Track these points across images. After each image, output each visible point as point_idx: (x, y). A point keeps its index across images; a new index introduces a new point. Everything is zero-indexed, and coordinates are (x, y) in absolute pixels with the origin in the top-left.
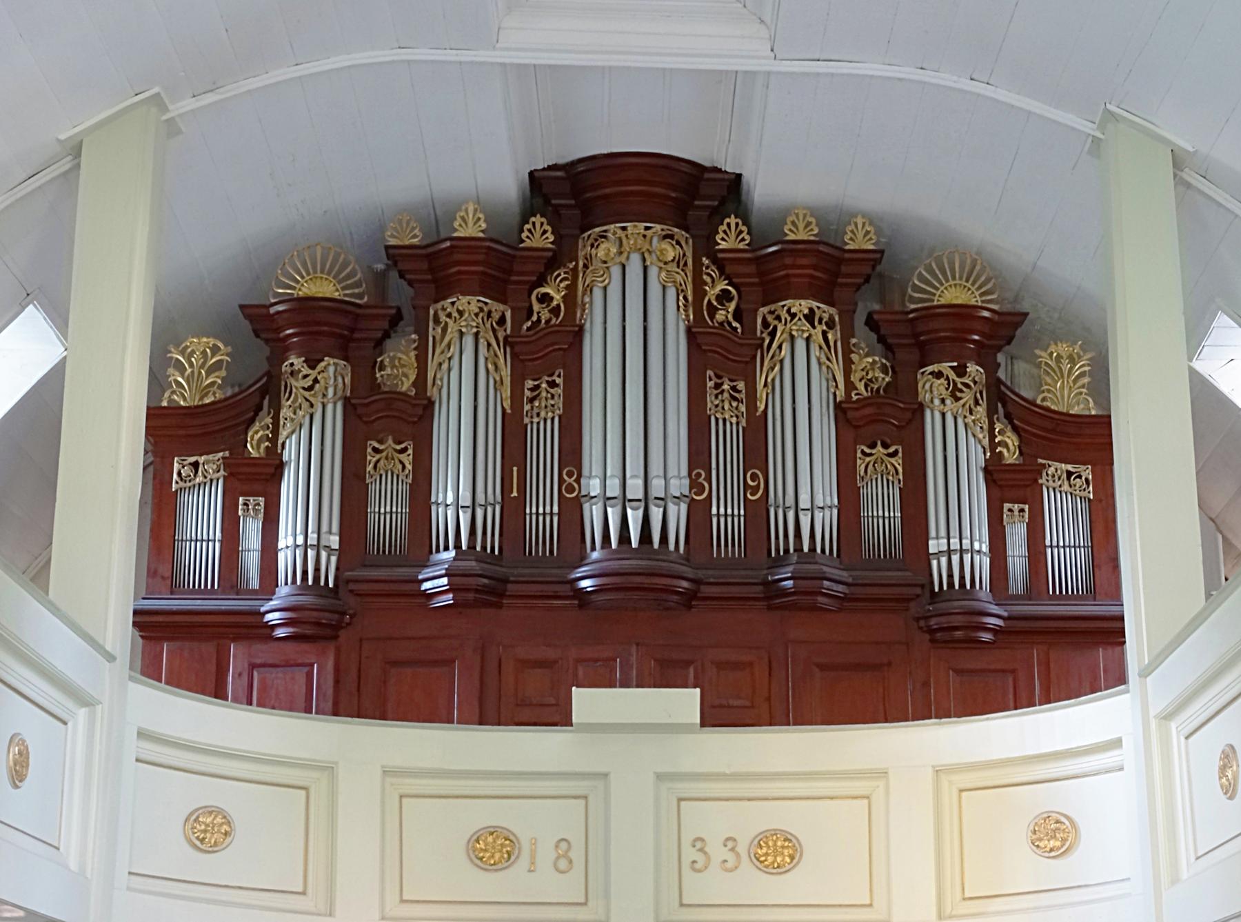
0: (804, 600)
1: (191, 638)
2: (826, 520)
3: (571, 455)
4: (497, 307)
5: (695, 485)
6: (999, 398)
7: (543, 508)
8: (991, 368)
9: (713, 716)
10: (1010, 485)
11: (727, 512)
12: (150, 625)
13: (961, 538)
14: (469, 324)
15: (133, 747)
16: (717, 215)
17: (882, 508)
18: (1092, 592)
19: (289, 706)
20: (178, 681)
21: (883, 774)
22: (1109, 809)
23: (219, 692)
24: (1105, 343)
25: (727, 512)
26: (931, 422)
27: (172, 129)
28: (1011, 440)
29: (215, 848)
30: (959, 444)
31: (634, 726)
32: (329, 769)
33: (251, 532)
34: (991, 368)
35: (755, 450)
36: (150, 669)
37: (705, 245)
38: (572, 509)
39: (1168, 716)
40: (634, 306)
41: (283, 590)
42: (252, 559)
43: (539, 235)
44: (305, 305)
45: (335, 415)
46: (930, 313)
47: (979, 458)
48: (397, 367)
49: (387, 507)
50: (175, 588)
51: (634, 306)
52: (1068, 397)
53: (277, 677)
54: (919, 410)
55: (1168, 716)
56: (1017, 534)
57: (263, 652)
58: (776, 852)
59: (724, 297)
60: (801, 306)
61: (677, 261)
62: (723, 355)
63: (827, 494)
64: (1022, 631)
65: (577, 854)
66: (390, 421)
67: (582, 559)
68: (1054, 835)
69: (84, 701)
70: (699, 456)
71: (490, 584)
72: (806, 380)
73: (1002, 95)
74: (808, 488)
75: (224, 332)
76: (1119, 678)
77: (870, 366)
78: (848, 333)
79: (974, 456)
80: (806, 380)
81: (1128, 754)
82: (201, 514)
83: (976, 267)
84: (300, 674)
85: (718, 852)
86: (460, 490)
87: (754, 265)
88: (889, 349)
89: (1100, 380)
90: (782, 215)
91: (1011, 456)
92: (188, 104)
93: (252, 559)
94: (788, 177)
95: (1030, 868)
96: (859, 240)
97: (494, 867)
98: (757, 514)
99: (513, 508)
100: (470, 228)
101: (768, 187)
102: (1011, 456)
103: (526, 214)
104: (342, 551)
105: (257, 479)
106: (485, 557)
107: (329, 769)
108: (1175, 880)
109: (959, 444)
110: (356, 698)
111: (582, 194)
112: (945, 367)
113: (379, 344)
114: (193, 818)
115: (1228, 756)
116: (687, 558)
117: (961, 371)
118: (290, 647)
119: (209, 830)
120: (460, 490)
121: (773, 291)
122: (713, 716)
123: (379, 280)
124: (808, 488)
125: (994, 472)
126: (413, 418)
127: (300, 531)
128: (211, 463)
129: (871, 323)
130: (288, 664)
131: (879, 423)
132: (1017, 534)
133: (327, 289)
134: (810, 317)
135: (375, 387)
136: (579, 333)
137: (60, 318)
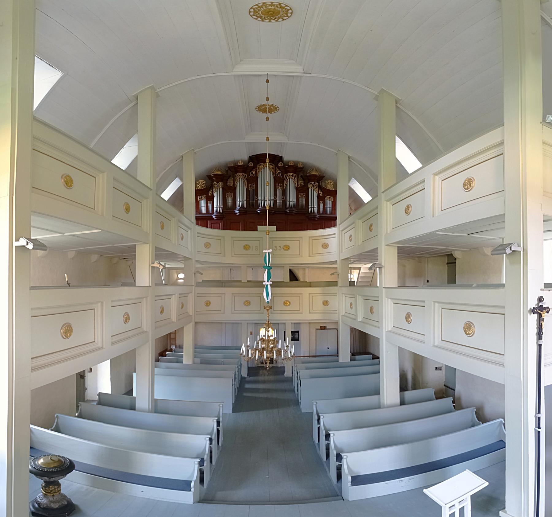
0: (291, 214)
1: (203, 220)
2: (294, 203)
3: (256, 194)
4: (245, 175)
5: (275, 198)
6: (320, 187)
7: (252, 201)
8: (319, 183)
9: (278, 230)
10: (321, 199)
11: (279, 202)
12: (197, 219)
13: (314, 206)
14: (241, 177)
15: (197, 235)
16: (278, 162)
17: (302, 201)
18: (332, 213)
19: (217, 229)
20: (201, 225)
21: (302, 238)
22: (333, 243)
23: (207, 227)
24: (336, 180)
25: (279, 202)
26: (310, 190)
27: (195, 153)
28: (321, 193)
29: (209, 248)
30: (314, 193)
31: (267, 231)
32: (224, 237)
33: (210, 206)
34: (319, 183)
35: (284, 193)
36: (197, 224)
37: (276, 166)
38: (257, 201)
39: (342, 231)
40: (266, 175)
41: (215, 213)
42: (210, 209)
43: (251, 165)
44: (216, 175)
45: (221, 190)
46: (310, 176)
47: (317, 195)
48: (230, 183)
49: (229, 201)
50: (200, 213)
51: (266, 175)
52: (330, 187)
53: (215, 225)
54: (308, 189)
55: (342, 231)
56: (321, 205)
57: (213, 221)
58: (287, 248)
59: (279, 173)
60: (291, 174)
61: (273, 168)
62: (279, 181)
63: (294, 199)
64: (321, 218)
65: (258, 248)
66: (229, 190)
67: (258, 208)
68: (325, 246)
69: (190, 229)
70: (275, 194)
71: (245, 211)
72: (291, 185)
73: (323, 147)
74: (291, 199)
75: (204, 179)
76: (335, 225)
77: (301, 182)
78: (298, 178)
79: (316, 195)
80: (291, 185)
81: (336, 236)
82: (203, 203)
83: (317, 170)
84: (218, 225)
85: (278, 248)
86: (240, 200)
87: (283, 168)
88: (304, 180)
89: (335, 185)
90: (289, 162)
91: (321, 195)
92: (198, 150)
93: (210, 209)
94: (289, 156)
95: (321, 250)
96: (300, 165)
97: (247, 250)
98: (284, 202)
99: (248, 201)
100: (240, 164)
101: (286, 158)
102: (321, 195)
103: (249, 162)
104: (223, 208)
105: (210, 199)
106: (244, 208)
107: (224, 237)
108: (342, 252)
109: (314, 193)
110: (226, 227)
111: (257, 160)
112: (312, 183)
113: (227, 180)
114: (205, 244)
115: (351, 236)
116: (274, 208)
117: (314, 183)
118: (217, 221)
119: (207, 245)
120: (240, 200)
121: (287, 172)
122: (278, 230)
123: (227, 171)
124: (291, 199)
125: (319, 197)
126: (233, 190)
127: (217, 205)
128: (204, 197)
129: (301, 176)
130: (216, 223)
131: (302, 190)
132: (321, 205)
133: (219, 173)
134: (292, 176)
135: (227, 186)
136: (257, 178)
137: (182, 179)
